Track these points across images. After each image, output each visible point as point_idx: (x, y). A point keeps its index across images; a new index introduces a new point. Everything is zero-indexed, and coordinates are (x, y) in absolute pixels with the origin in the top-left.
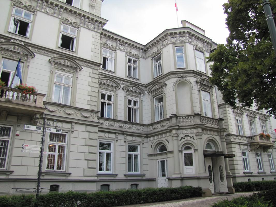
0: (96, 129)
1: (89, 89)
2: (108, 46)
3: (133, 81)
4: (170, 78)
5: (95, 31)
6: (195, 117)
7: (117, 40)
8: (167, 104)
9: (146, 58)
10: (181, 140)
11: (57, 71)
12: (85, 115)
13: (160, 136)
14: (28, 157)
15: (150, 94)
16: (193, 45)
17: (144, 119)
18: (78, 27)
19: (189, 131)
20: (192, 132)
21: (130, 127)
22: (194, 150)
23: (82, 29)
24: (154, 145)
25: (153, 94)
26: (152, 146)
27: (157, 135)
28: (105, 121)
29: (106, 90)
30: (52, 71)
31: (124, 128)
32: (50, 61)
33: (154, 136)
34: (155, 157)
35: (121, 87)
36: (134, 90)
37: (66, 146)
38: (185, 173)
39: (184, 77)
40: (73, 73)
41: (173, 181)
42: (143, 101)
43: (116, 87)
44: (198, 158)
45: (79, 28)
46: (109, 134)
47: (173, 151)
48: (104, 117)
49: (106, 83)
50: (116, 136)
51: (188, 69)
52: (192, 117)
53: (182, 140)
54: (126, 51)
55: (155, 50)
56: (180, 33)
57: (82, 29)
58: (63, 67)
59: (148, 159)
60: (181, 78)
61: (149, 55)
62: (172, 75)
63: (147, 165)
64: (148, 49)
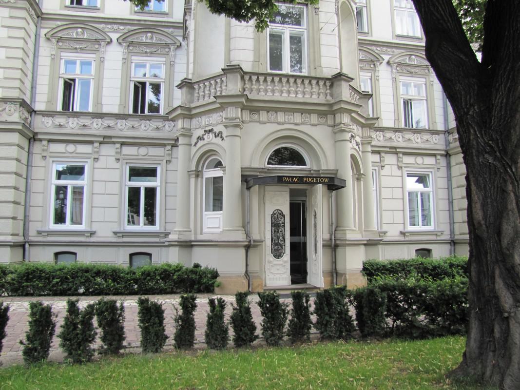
3: (145, 21)
17: (105, 101)
21: (157, 128)
28: (414, 134)
29: (410, 75)
32: (120, 41)
38: (205, 230)
43: (169, 45)
46: (424, 158)
48: (71, 110)
49: (75, 37)
51: (103, 12)
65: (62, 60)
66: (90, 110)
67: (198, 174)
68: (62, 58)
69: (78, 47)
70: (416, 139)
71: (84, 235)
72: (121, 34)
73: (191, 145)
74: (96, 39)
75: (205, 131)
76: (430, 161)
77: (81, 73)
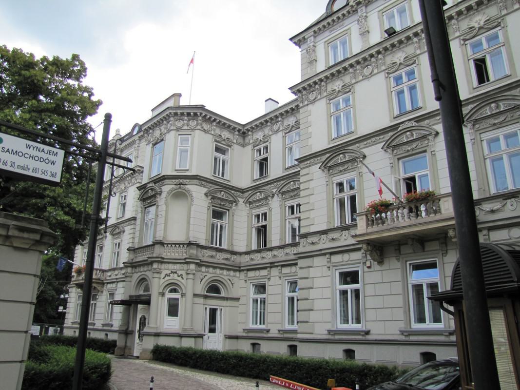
10: (164, 278)
16: (213, 135)
19: (177, 267)
36: (223, 196)
38: (165, 326)
41: (184, 339)
42: (235, 214)
52: (185, 246)
53: (165, 278)
54: (281, 128)
55: (259, 135)
56: (189, 114)
60: (179, 186)
62: (167, 180)
63: (240, 313)
65: (483, 142)
66: (493, 191)
67: (163, 294)
68: (482, 139)
69: (409, 148)
71: (360, 334)
72: (321, 164)
73: (160, 278)
74: (423, 136)
76: (357, 255)
77: (491, 152)
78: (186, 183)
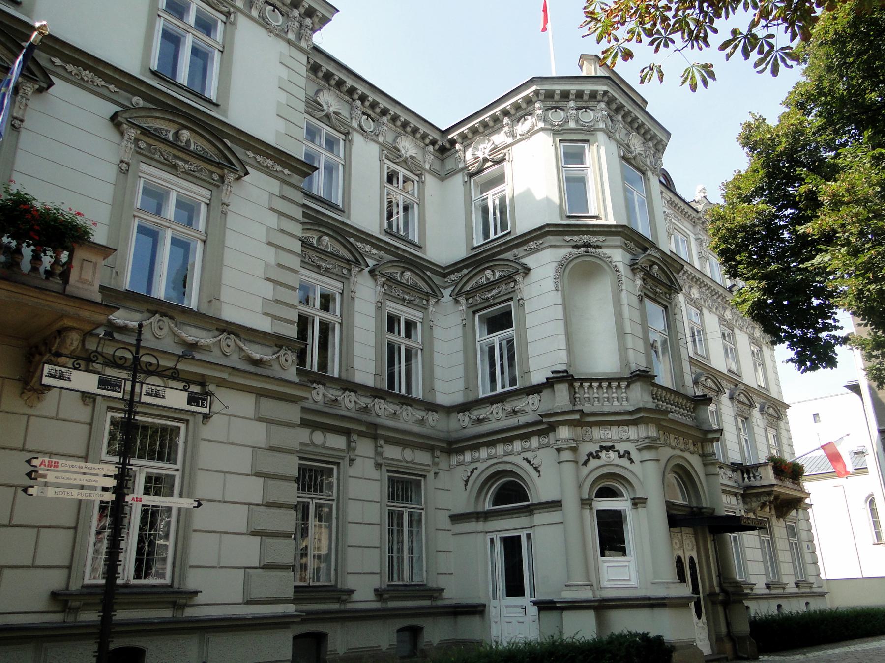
0: (293, 413)
1: (270, 255)
2: (324, 113)
3: (404, 251)
4: (542, 246)
5: (289, 42)
6: (633, 386)
7: (356, 96)
8: (531, 335)
9: (443, 175)
11: (143, 167)
12: (257, 356)
13: (500, 449)
14: (220, 502)
15: (460, 299)
17: (438, 385)
18: (226, 10)
19: (613, 433)
20: (625, 438)
21: (395, 413)
22: (633, 499)
23: (242, 22)
24: (476, 481)
25: (471, 300)
26: (467, 482)
27: (491, 444)
30: (128, 164)
31: (374, 414)
33: (476, 448)
34: (481, 523)
35: (368, 266)
37: (178, 475)
39: (591, 246)
40: (211, 187)
44: (645, 528)
45: (232, 16)
47: (561, 502)
50: (349, 442)
52: (624, 384)
56: (579, 95)
57: (242, 22)
58: (173, 155)
59: (450, 533)
61: (457, 165)
64: (453, 142)
70: (377, 407)
75: (601, 447)
78: (599, 244)
